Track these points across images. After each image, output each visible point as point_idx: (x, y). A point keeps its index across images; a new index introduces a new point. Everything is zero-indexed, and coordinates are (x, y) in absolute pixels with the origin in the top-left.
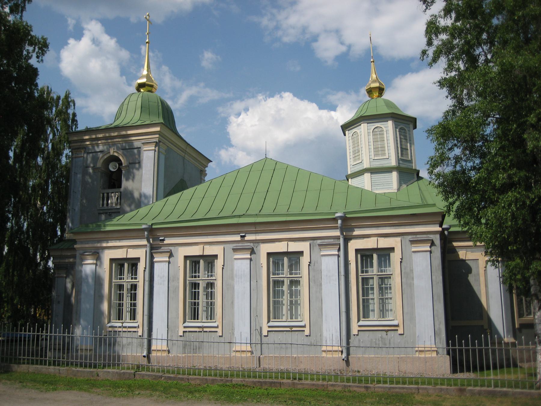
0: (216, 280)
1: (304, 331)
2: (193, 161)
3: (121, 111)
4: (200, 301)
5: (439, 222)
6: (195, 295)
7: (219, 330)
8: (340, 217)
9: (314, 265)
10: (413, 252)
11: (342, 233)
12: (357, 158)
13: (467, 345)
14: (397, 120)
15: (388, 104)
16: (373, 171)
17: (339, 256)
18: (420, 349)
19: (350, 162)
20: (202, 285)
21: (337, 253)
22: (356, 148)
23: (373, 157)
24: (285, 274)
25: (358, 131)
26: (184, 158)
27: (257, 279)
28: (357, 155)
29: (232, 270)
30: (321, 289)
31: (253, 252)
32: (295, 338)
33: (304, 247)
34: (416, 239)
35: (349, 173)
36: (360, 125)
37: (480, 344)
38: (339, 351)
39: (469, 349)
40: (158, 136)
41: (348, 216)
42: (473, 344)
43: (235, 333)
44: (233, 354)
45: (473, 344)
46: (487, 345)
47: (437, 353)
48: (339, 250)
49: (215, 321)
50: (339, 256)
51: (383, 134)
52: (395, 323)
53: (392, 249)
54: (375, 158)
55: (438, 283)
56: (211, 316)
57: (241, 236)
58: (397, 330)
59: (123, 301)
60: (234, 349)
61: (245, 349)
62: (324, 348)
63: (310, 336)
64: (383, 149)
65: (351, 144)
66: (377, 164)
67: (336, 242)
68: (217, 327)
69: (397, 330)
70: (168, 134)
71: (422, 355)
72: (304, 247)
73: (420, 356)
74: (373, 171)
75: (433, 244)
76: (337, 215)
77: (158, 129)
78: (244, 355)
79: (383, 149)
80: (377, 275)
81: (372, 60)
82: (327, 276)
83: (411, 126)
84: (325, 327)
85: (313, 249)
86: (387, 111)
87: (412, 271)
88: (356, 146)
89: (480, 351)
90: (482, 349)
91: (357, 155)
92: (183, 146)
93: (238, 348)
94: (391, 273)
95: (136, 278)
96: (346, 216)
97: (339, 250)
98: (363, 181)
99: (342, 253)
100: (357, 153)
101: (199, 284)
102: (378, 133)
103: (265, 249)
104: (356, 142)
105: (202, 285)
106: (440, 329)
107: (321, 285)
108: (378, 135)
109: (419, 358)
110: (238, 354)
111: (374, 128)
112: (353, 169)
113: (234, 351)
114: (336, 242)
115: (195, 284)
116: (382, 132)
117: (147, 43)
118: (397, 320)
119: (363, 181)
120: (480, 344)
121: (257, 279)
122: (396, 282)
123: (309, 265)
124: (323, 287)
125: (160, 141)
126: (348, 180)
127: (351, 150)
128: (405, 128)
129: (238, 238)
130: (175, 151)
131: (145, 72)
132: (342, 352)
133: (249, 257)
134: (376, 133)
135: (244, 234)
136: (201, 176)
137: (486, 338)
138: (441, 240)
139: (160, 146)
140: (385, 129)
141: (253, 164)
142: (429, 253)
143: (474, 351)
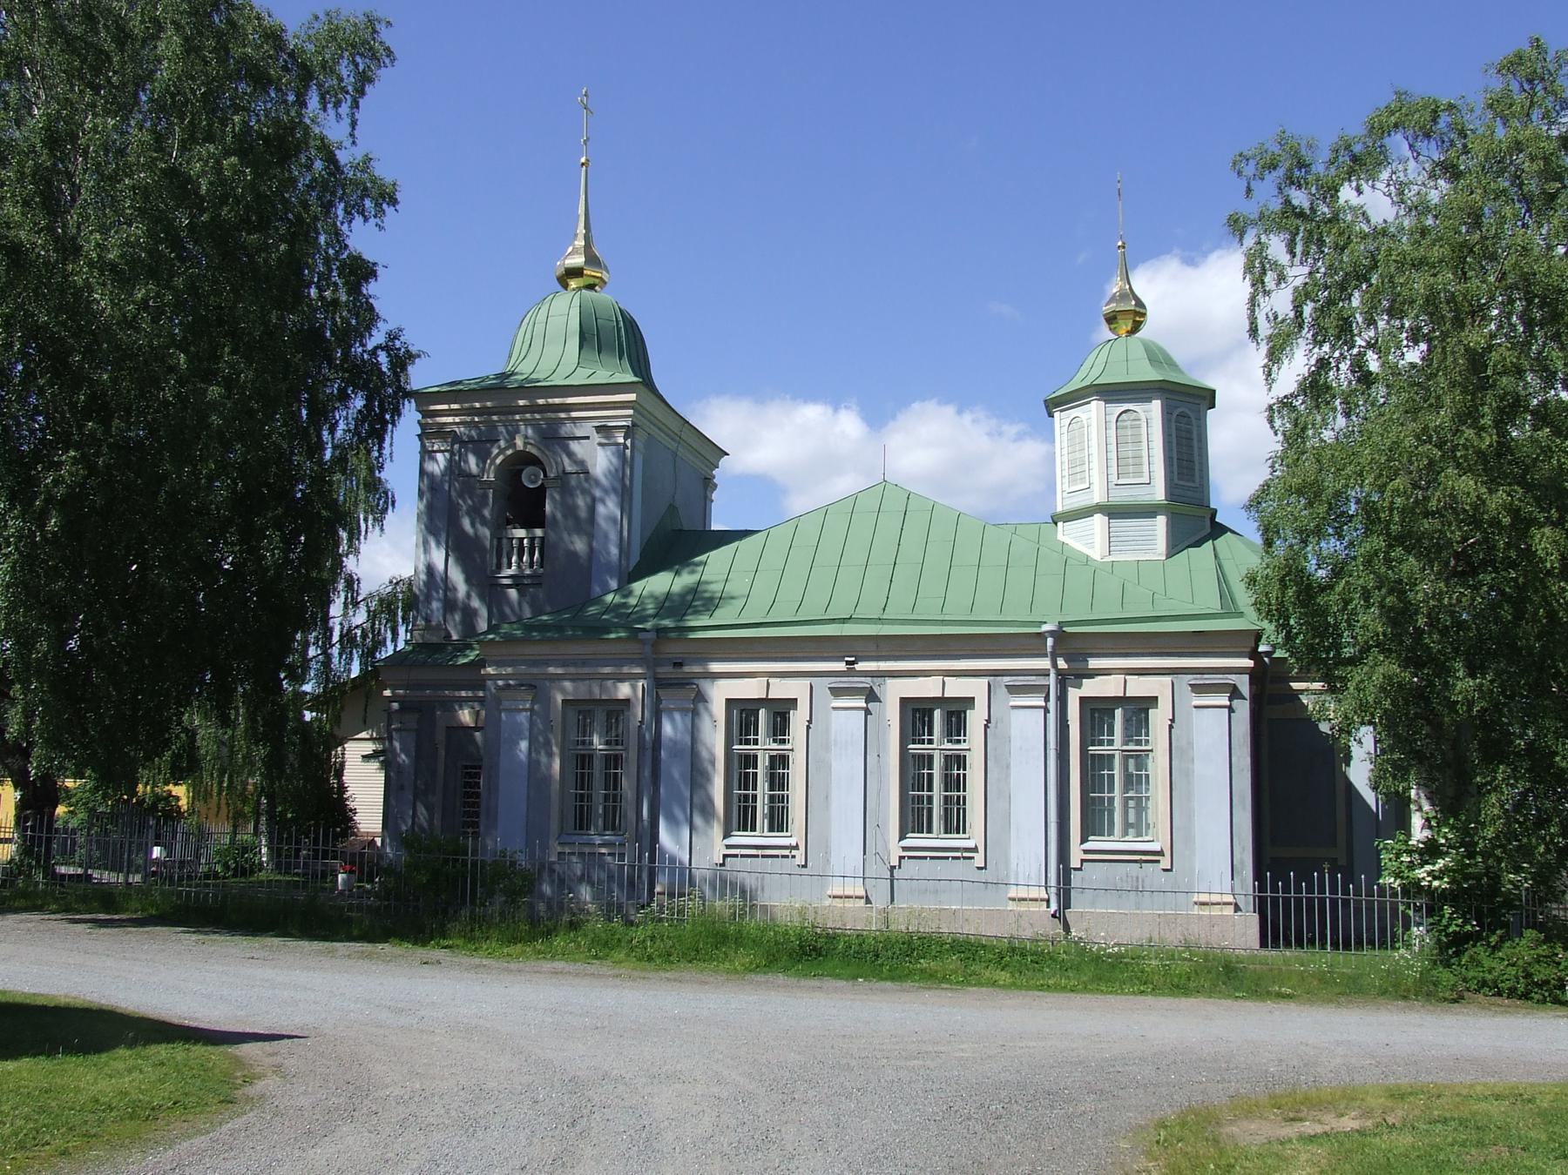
0: (792, 750)
1: (973, 858)
2: (691, 458)
3: (528, 336)
4: (759, 792)
5: (1248, 650)
6: (748, 781)
7: (800, 854)
8: (1052, 633)
9: (996, 727)
10: (1196, 707)
11: (1054, 664)
12: (1078, 476)
13: (1286, 889)
14: (1169, 396)
15: (1156, 356)
16: (1114, 512)
17: (1047, 711)
18: (1204, 898)
19: (1062, 485)
20: (763, 762)
21: (1043, 704)
22: (1077, 455)
23: (1113, 478)
24: (938, 745)
25: (1084, 417)
26: (675, 454)
27: (879, 750)
28: (1078, 469)
29: (827, 731)
30: (1008, 776)
31: (871, 696)
32: (958, 869)
33: (974, 688)
34: (1201, 682)
35: (1059, 509)
36: (1089, 403)
37: (1310, 890)
38: (1042, 900)
39: (1278, 897)
40: (631, 412)
41: (1068, 629)
42: (1298, 890)
43: (833, 860)
44: (828, 902)
45: (1298, 890)
46: (1322, 891)
47: (1237, 908)
48: (1047, 699)
49: (789, 834)
50: (1047, 711)
51: (1139, 427)
52: (1155, 847)
53: (1153, 701)
54: (1120, 482)
55: (1243, 770)
56: (778, 821)
57: (848, 663)
58: (1158, 861)
59: (755, 788)
60: (829, 892)
61: (851, 893)
62: (1013, 893)
63: (985, 868)
64: (1137, 460)
65: (1065, 444)
66: (1122, 496)
67: (1041, 681)
68: (796, 847)
69: (1158, 861)
70: (651, 404)
71: (1205, 912)
72: (974, 688)
73: (1201, 913)
74: (1114, 512)
75: (1235, 693)
76: (1045, 628)
77: (632, 397)
78: (849, 904)
79: (1137, 460)
80: (1123, 751)
81: (1120, 243)
82: (1021, 748)
83: (1207, 403)
84: (1014, 852)
85: (995, 693)
86: (1150, 374)
87: (1190, 744)
88: (1077, 448)
89: (1310, 901)
90: (1302, 898)
91: (1078, 469)
92: (674, 425)
93: (1012, 894)
94: (1150, 748)
95: (783, 742)
96: (1064, 629)
97: (1047, 699)
98: (1091, 532)
99: (1052, 705)
100: (1077, 468)
101: (756, 757)
102: (1128, 423)
103: (893, 692)
104: (1077, 441)
105: (763, 762)
106: (1242, 862)
107: (1008, 767)
108: (1123, 428)
109: (1200, 917)
110: (838, 903)
111: (1121, 414)
112: (1067, 502)
113: (1196, 903)
114: (1041, 681)
115: (747, 757)
116: (1138, 422)
117: (583, 164)
118: (1158, 841)
119: (1091, 532)
120: (1310, 890)
121: (879, 750)
122: (1158, 766)
123: (986, 727)
124: (1013, 770)
125: (634, 425)
126: (1056, 524)
127: (1065, 459)
128: (1189, 413)
129: (841, 666)
130: (659, 439)
131: (580, 243)
132: (1048, 901)
133: (865, 705)
134: (1125, 424)
135: (853, 659)
136: (706, 489)
137: (1322, 878)
138: (1251, 684)
139: (637, 436)
140: (1143, 416)
141: (856, 496)
142: (1226, 710)
143: (1299, 901)
